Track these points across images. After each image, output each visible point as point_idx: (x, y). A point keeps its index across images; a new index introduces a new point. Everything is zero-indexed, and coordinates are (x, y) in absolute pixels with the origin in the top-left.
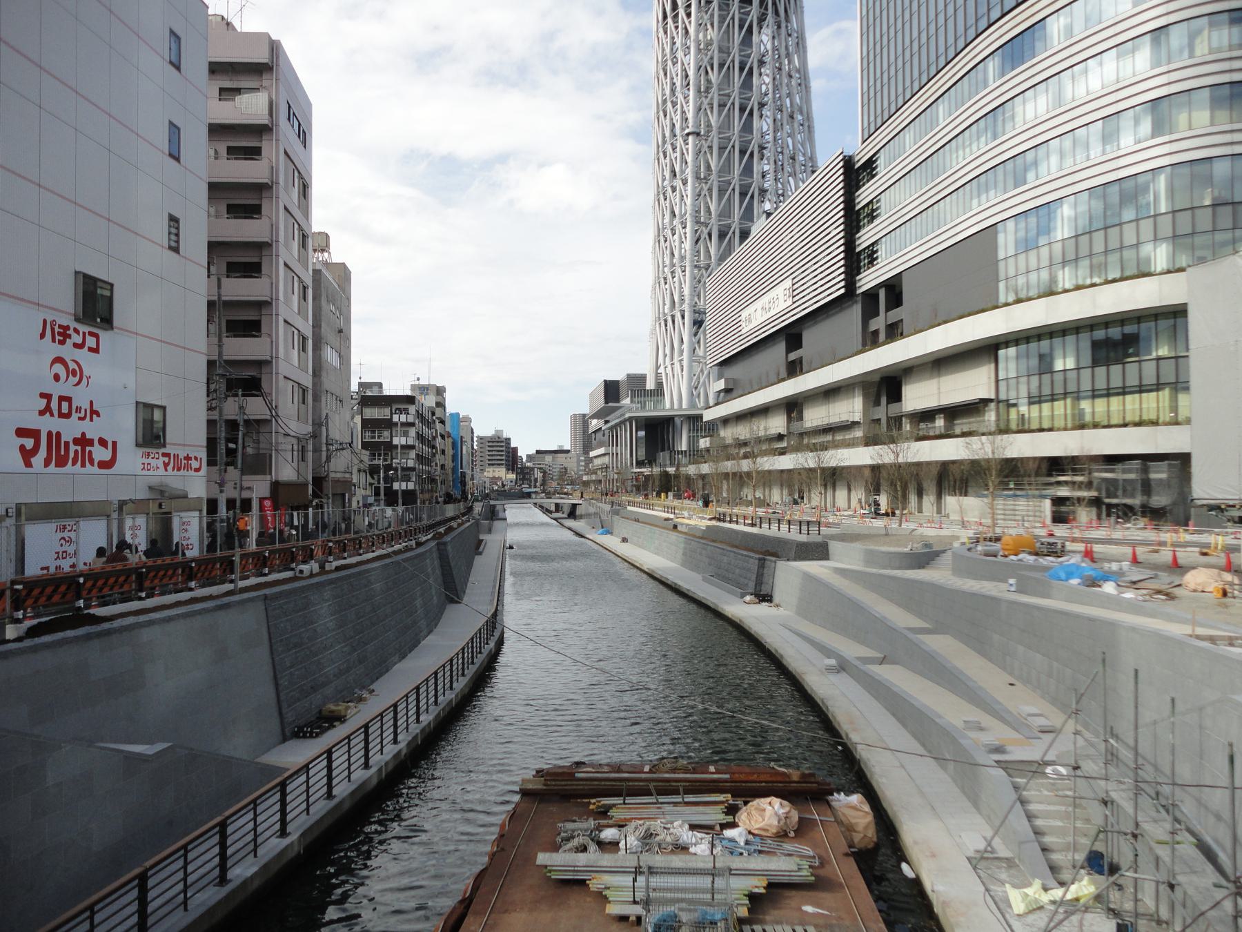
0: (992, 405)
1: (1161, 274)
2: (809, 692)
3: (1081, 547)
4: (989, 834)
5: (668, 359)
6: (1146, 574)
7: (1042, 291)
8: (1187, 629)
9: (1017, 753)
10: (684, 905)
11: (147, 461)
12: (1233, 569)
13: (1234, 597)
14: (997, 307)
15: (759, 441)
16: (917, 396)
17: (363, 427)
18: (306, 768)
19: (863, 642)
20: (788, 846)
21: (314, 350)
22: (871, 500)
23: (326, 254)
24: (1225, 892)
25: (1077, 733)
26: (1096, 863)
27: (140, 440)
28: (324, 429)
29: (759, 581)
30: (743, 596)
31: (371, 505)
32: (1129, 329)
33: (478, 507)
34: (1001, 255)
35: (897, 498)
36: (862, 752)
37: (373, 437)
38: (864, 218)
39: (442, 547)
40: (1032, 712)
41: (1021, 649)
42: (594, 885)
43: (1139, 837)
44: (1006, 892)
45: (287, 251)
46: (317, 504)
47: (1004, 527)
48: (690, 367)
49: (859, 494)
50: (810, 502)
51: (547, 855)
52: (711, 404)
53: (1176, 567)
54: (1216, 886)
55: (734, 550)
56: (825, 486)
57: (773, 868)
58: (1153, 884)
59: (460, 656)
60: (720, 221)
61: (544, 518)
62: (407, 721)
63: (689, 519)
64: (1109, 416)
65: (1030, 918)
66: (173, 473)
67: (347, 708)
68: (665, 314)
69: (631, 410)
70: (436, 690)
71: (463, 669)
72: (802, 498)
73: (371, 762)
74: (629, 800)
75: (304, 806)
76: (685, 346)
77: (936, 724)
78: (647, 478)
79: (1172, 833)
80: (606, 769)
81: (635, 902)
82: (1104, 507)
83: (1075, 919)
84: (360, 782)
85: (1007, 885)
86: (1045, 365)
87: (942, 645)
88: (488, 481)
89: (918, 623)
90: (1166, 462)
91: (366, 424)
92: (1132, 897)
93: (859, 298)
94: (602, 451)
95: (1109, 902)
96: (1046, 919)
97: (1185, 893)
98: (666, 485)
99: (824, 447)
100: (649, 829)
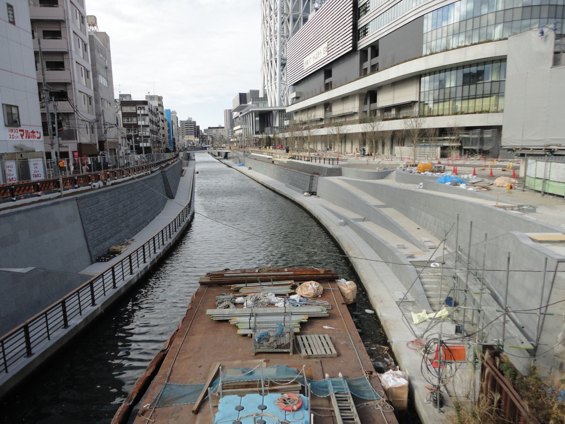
0: (417, 104)
1: (496, 41)
2: (332, 234)
3: (452, 168)
4: (406, 291)
5: (269, 82)
6: (479, 179)
7: (442, 49)
8: (494, 203)
9: (420, 258)
10: (271, 329)
11: (12, 134)
12: (516, 177)
13: (515, 189)
14: (421, 57)
15: (312, 122)
16: (384, 100)
17: (123, 117)
18: (102, 275)
19: (356, 212)
20: (318, 301)
21: (93, 77)
22: (362, 148)
23: (95, 27)
24: (501, 313)
25: (444, 249)
26: (449, 302)
27: (7, 124)
28: (102, 117)
29: (311, 186)
30: (303, 193)
31: (129, 154)
32: (480, 68)
33: (181, 154)
34: (425, 30)
35: (373, 148)
36: (353, 260)
37: (128, 121)
38: (362, 11)
39: (164, 173)
40: (426, 240)
41: (423, 213)
42: (232, 322)
43: (468, 292)
44: (411, 315)
45: (73, 25)
46: (102, 154)
47: (419, 160)
48: (280, 86)
49: (356, 146)
50: (334, 150)
51: (211, 310)
52: (290, 104)
53: (492, 176)
54: (497, 311)
55: (299, 172)
56: (341, 142)
57: (311, 311)
58: (472, 310)
59: (174, 223)
60: (293, 13)
61: (213, 159)
62: (150, 253)
63: (279, 158)
64: (468, 109)
65: (421, 325)
66: (26, 140)
67: (121, 248)
68: (267, 60)
69: (252, 107)
70: (163, 238)
71: (175, 229)
72: (331, 148)
73: (133, 271)
74: (248, 285)
75: (103, 292)
76: (277, 76)
77: (386, 246)
78: (260, 140)
79: (481, 290)
80: (239, 272)
81: (250, 328)
82: (463, 150)
83: (439, 325)
84: (129, 280)
85: (412, 312)
86: (442, 84)
87: (390, 213)
88: (186, 142)
89: (379, 203)
90: (491, 130)
91: (125, 115)
92: (463, 315)
93: (359, 53)
94: (239, 127)
95: (453, 317)
96: (427, 326)
97: (484, 313)
98: (269, 142)
99: (341, 125)
100: (257, 297)
